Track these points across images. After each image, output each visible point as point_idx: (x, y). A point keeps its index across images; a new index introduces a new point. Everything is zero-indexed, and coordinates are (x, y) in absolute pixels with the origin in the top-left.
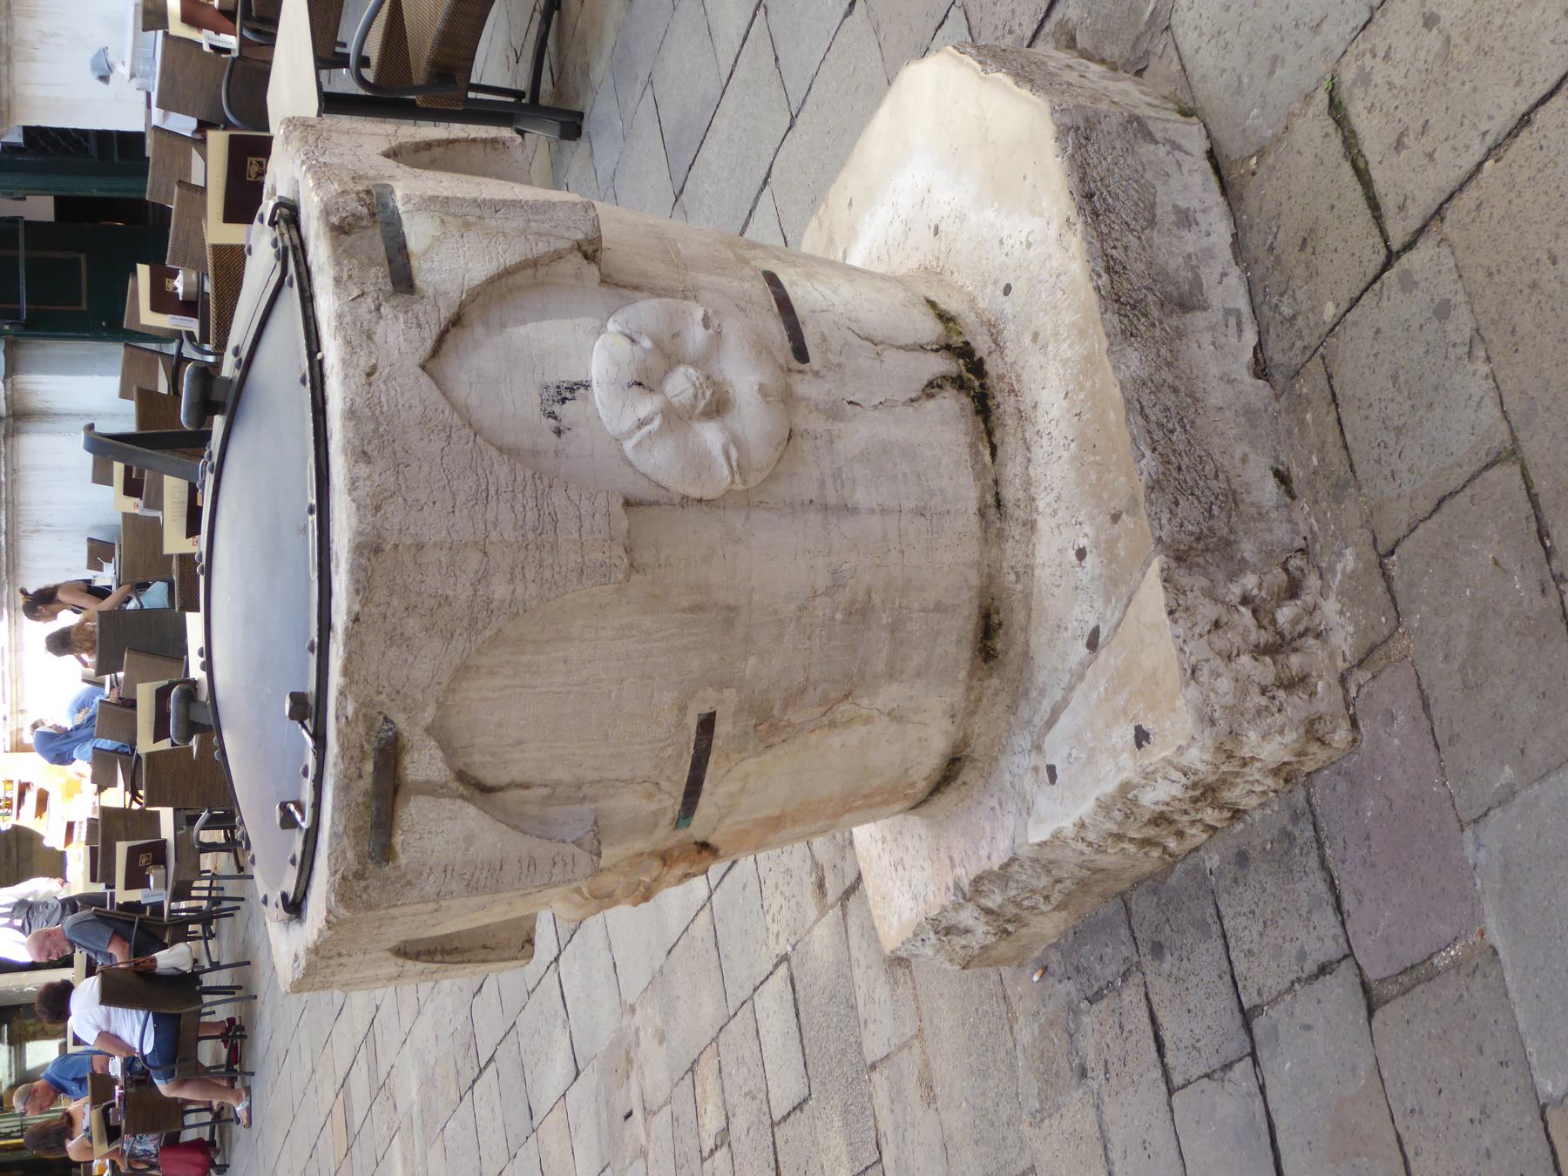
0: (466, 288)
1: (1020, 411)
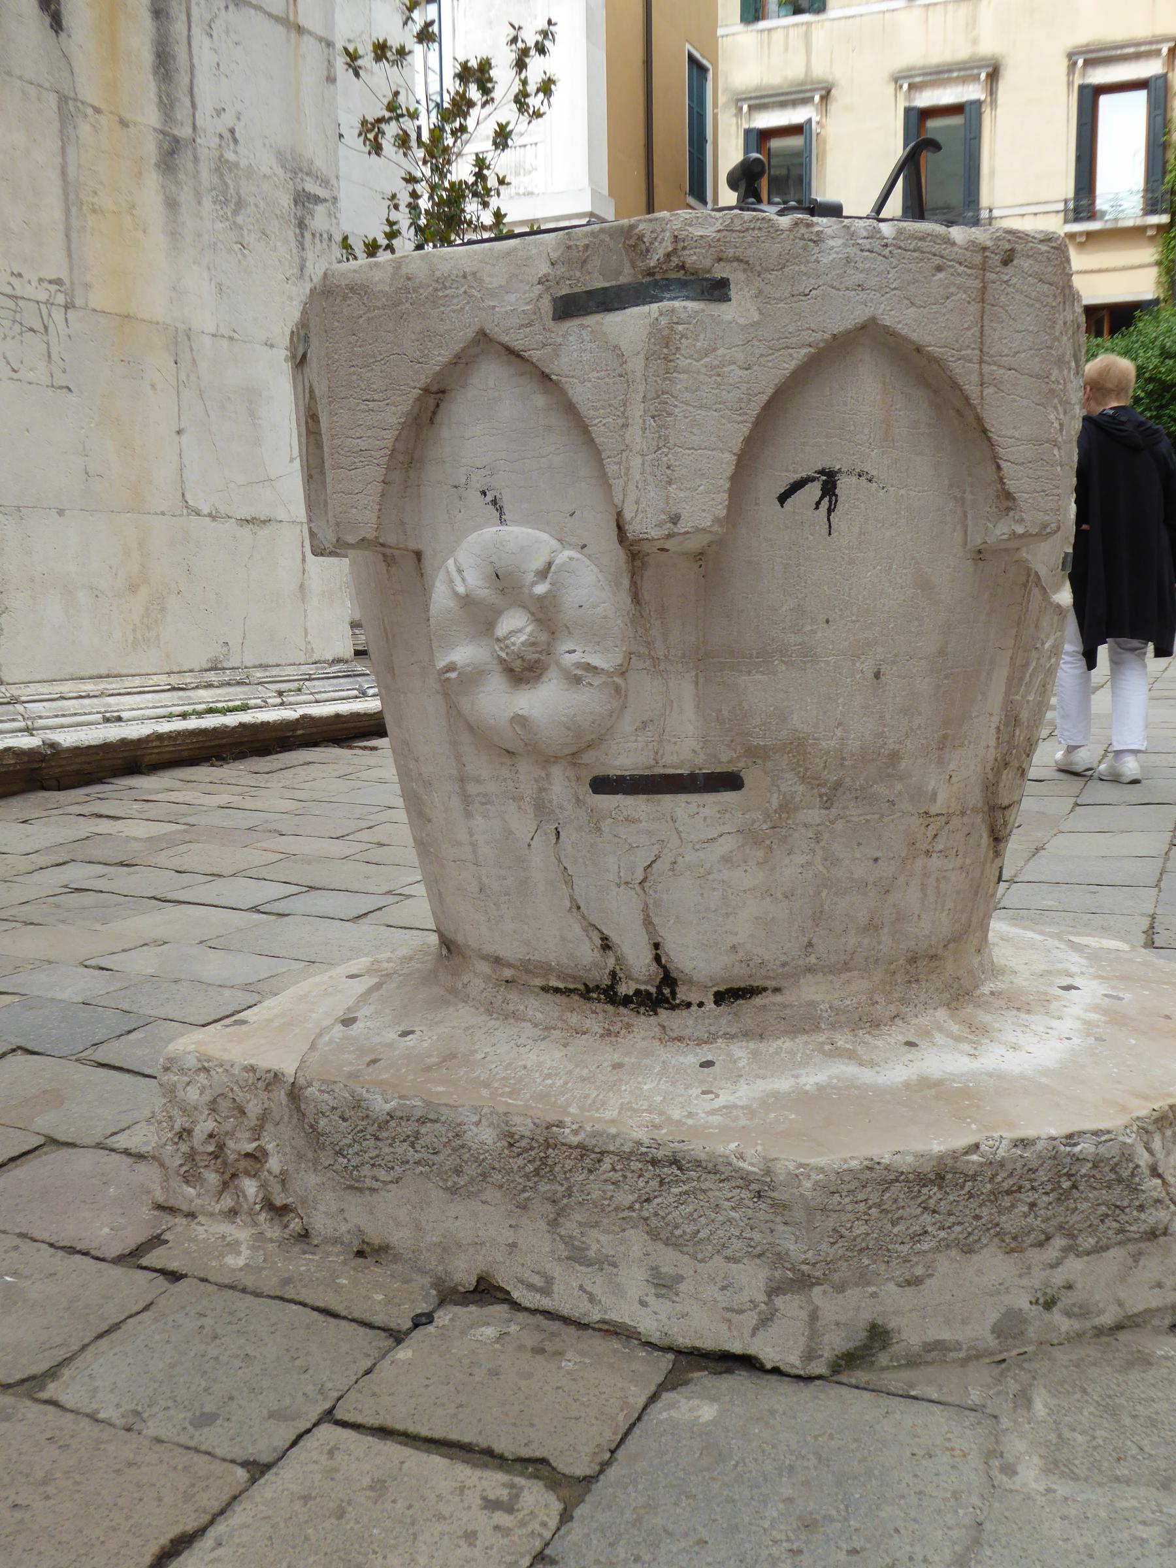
0: (564, 380)
1: (584, 1033)
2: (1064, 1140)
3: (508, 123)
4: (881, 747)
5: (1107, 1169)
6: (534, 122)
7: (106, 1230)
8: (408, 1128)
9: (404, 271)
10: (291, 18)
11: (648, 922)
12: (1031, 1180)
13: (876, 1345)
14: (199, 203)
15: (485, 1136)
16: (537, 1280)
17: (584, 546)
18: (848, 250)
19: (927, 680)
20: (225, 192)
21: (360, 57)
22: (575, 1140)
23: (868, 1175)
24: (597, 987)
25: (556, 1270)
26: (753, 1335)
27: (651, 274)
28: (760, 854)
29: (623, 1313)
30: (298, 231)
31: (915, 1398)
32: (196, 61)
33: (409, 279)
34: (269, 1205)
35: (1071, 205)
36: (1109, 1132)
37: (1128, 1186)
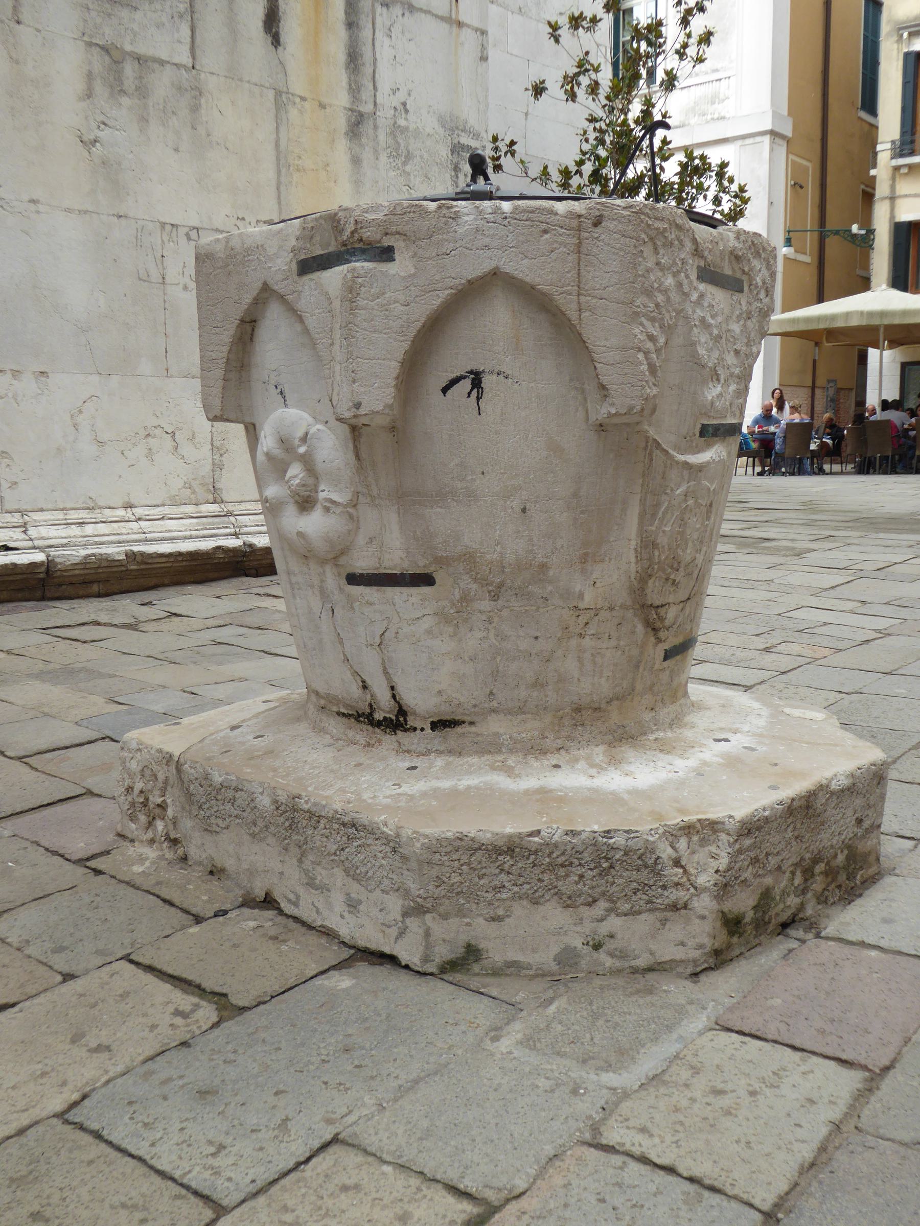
2: (602, 834)
3: (672, 69)
4: (532, 560)
5: (635, 857)
6: (698, 66)
7: (82, 844)
8: (230, 794)
9: (231, 244)
10: (454, 16)
11: (386, 672)
12: (578, 859)
13: (471, 958)
14: (377, 159)
15: (265, 801)
16: (292, 897)
17: (327, 422)
18: (478, 223)
19: (565, 514)
20: (397, 150)
21: (560, 28)
22: (306, 807)
23: (459, 843)
24: (363, 713)
25: (301, 891)
26: (395, 943)
27: (345, 245)
28: (451, 630)
29: (332, 921)
30: (453, 174)
31: (482, 993)
32: (378, 56)
33: (232, 249)
34: (168, 838)
35: (898, 143)
36: (637, 832)
37: (652, 871)
